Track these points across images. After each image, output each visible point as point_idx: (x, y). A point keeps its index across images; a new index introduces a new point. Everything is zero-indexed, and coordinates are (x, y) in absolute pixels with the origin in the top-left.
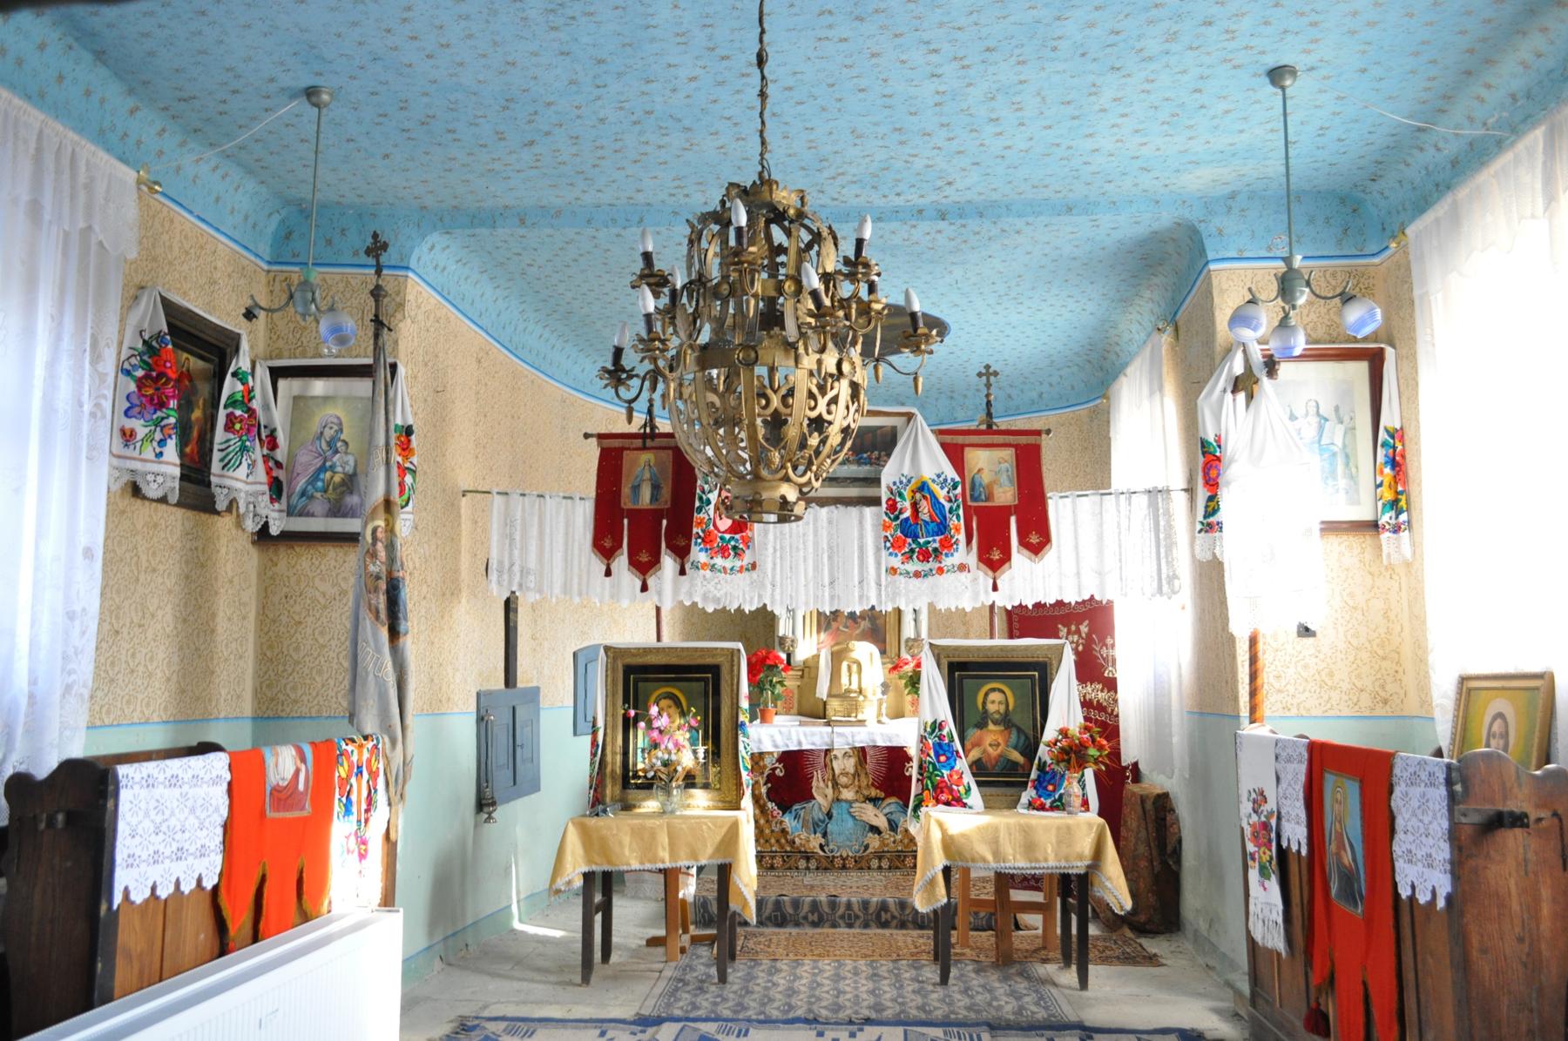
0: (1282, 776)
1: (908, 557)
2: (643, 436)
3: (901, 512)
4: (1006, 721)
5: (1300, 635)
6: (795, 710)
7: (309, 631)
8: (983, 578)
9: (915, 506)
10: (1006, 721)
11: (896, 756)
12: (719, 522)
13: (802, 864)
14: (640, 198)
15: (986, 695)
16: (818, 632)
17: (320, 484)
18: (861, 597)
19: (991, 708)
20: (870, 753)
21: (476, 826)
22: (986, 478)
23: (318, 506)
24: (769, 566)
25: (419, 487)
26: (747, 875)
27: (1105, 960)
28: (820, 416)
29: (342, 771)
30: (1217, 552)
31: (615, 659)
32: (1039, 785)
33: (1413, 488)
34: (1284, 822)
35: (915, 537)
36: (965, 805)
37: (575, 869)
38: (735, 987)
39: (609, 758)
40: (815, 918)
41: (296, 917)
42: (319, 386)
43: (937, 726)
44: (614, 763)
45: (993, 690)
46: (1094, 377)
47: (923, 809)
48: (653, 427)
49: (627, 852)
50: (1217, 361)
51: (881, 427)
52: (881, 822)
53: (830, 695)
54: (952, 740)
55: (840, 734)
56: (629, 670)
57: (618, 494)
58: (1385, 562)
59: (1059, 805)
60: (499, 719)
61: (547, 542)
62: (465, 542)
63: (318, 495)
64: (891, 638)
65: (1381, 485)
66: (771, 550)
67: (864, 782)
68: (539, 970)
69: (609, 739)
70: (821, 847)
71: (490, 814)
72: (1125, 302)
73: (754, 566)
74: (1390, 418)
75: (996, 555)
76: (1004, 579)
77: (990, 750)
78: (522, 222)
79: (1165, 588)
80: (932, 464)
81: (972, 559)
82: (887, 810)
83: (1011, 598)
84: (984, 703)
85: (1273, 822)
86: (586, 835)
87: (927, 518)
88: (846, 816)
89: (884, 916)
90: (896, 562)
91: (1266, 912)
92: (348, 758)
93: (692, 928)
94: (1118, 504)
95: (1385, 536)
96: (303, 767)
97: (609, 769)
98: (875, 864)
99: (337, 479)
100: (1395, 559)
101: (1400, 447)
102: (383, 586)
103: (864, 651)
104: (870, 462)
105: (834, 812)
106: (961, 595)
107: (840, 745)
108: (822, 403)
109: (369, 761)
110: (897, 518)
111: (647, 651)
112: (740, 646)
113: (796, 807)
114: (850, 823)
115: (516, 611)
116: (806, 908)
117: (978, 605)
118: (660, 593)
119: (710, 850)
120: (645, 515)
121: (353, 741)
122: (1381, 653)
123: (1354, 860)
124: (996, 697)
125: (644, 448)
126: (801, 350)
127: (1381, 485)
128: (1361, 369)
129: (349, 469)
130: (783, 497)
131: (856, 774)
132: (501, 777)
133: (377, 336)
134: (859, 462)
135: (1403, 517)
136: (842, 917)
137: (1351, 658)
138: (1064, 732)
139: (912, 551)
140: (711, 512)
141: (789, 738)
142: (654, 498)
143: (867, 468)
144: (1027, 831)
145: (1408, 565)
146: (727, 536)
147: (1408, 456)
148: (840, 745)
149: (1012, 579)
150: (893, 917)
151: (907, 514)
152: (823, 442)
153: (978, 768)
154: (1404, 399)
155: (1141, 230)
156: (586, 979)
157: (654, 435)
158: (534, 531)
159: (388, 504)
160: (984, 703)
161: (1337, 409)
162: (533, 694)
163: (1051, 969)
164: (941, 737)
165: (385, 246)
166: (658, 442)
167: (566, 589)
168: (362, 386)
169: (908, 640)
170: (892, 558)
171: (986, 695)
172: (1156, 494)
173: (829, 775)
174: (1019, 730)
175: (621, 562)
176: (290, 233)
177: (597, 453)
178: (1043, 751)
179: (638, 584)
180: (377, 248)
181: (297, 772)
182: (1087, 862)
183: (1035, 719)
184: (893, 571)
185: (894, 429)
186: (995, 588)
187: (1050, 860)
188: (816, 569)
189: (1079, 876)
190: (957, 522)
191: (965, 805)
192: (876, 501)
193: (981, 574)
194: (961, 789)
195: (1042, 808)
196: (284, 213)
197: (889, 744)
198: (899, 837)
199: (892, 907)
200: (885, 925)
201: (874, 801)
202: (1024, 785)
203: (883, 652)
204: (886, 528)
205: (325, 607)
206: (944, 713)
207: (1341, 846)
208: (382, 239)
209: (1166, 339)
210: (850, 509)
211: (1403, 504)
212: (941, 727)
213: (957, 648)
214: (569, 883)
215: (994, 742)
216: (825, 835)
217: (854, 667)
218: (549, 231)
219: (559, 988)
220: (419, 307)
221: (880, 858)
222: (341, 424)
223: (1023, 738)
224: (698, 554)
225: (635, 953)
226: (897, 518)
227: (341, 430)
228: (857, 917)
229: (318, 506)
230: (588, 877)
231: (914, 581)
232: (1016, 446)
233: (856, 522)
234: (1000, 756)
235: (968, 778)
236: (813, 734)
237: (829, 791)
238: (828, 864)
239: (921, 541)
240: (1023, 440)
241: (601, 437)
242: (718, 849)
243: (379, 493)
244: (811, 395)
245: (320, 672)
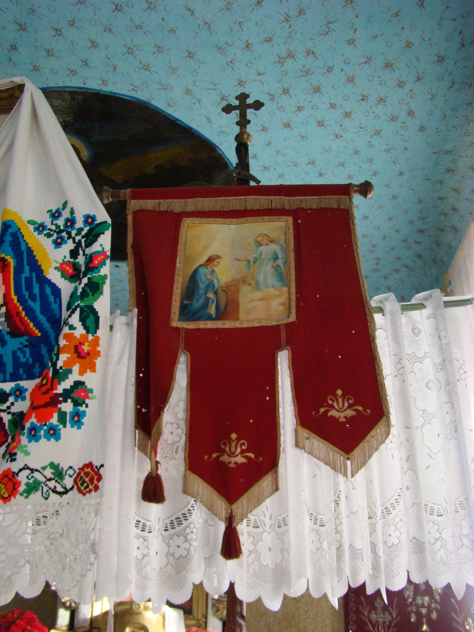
83: (281, 575)
186: (231, 548)
232: (295, 213)
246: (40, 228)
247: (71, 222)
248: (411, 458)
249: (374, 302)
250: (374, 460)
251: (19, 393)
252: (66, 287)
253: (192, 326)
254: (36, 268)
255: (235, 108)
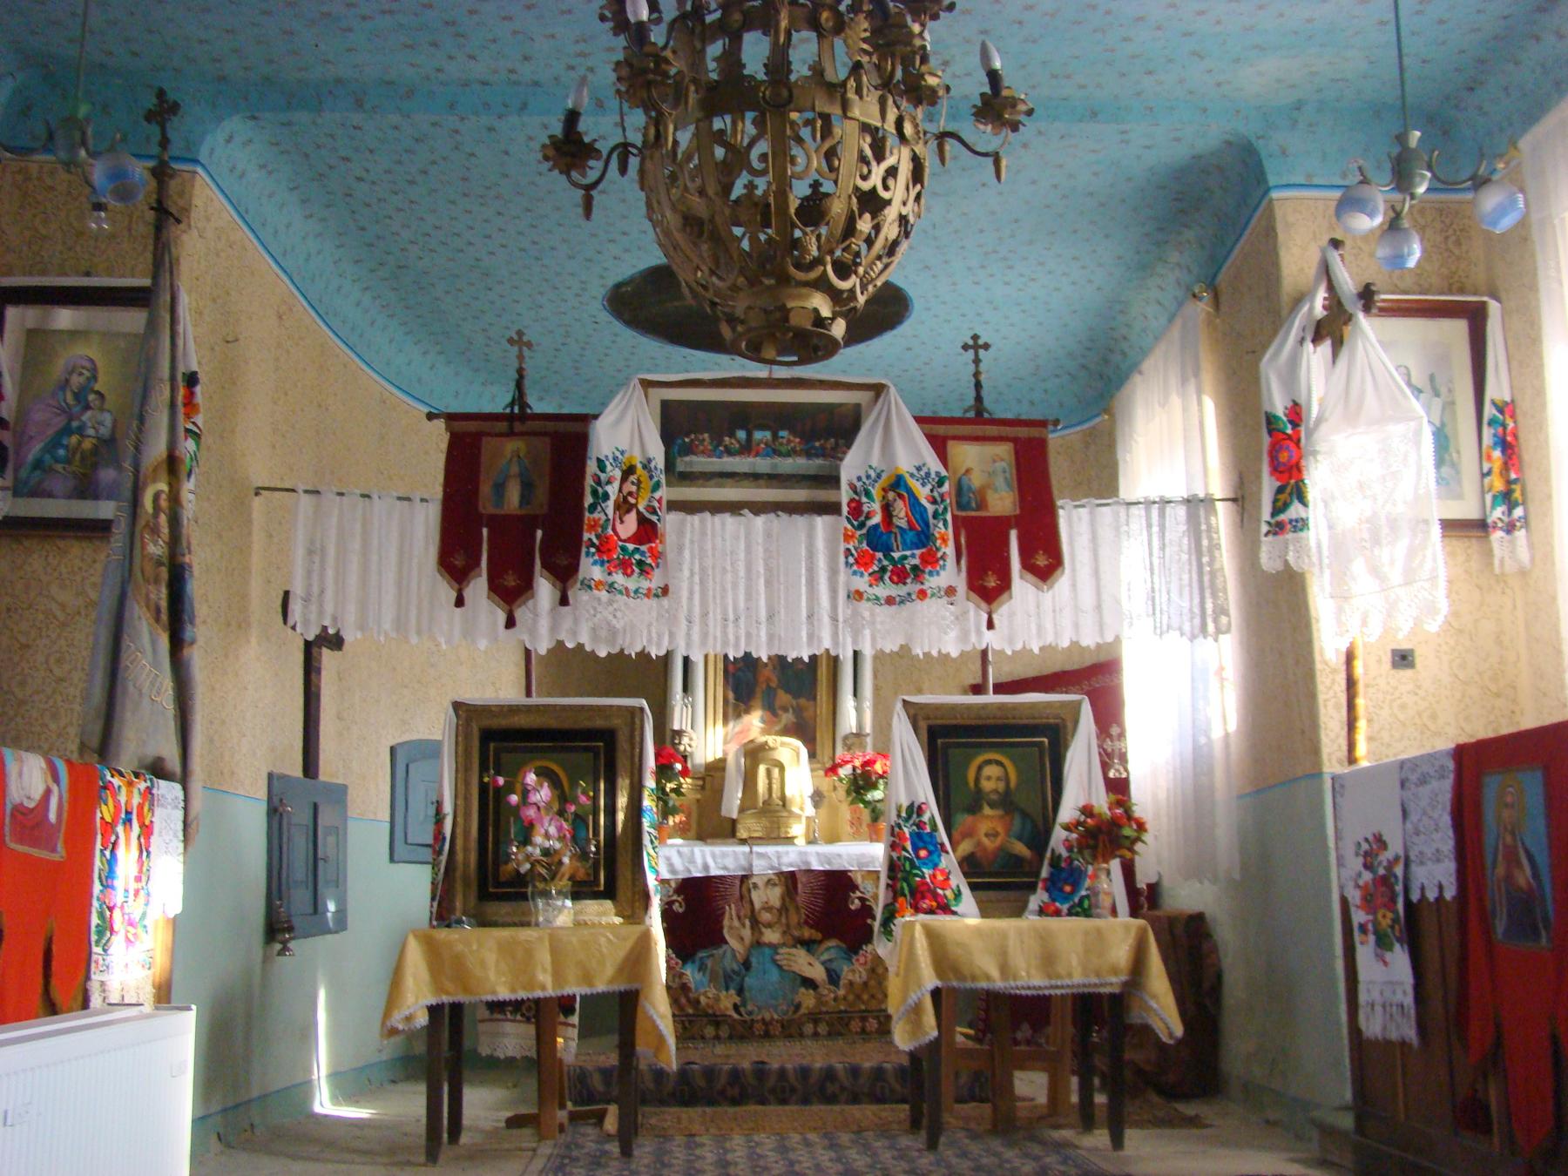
0: (1411, 807)
1: (878, 577)
2: (509, 418)
3: (868, 517)
4: (1006, 802)
5: (1395, 665)
6: (693, 832)
7: (40, 658)
8: (975, 613)
9: (887, 509)
10: (1006, 802)
11: (837, 883)
12: (619, 527)
13: (710, 1031)
14: (526, 72)
15: (980, 768)
16: (726, 720)
17: (62, 452)
18: (811, 636)
19: (987, 785)
20: (802, 879)
21: (266, 959)
22: (976, 480)
23: (59, 485)
24: (685, 594)
25: (203, 455)
26: (659, 1009)
27: (1139, 1125)
28: (874, 189)
29: (105, 812)
30: (1291, 558)
31: (468, 721)
32: (1053, 886)
33: (1531, 476)
34: (1414, 868)
35: (887, 551)
36: (954, 913)
37: (417, 999)
38: (646, 1161)
39: (460, 857)
40: (736, 1091)
41: (39, 1002)
42: (64, 318)
43: (915, 810)
44: (466, 864)
45: (989, 762)
46: (1100, 380)
47: (899, 921)
48: (524, 406)
49: (492, 976)
50: (1284, 312)
51: (841, 405)
52: (817, 972)
53: (742, 810)
54: (934, 828)
55: (761, 855)
56: (487, 736)
57: (475, 492)
58: (1497, 570)
59: (1083, 909)
60: (298, 815)
61: (375, 558)
62: (256, 561)
63: (59, 467)
64: (822, 736)
65: (1489, 473)
66: (686, 573)
67: (794, 919)
68: (355, 1151)
69: (459, 831)
70: (736, 1007)
71: (284, 943)
72: (1143, 268)
73: (665, 591)
74: (1497, 389)
75: (992, 582)
76: (1001, 614)
77: (986, 841)
78: (359, 104)
79: (1211, 627)
80: (911, 453)
81: (961, 583)
82: (825, 957)
83: (1011, 641)
84: (977, 780)
85: (1399, 870)
86: (433, 952)
87: (903, 524)
88: (769, 965)
89: (831, 1088)
90: (862, 583)
91: (1387, 994)
92: (114, 796)
93: (569, 1105)
94: (1148, 518)
95: (1497, 536)
96: (55, 789)
97: (459, 874)
98: (809, 1028)
99: (87, 444)
100: (1510, 567)
101: (1511, 425)
102: (164, 573)
103: (790, 752)
104: (823, 453)
105: (754, 960)
106: (942, 626)
107: (760, 868)
108: (878, 172)
109: (140, 807)
110: (862, 525)
111: (513, 710)
112: (644, 703)
113: (702, 954)
114: (774, 975)
115: (319, 671)
116: (723, 1080)
117: (969, 648)
118: (533, 631)
119: (610, 970)
120: (517, 509)
121: (121, 774)
122: (1494, 688)
123: (1536, 875)
124: (992, 772)
125: (511, 434)
126: (851, 95)
127: (1489, 473)
128: (1457, 329)
129: (104, 432)
130: (816, 311)
131: (784, 909)
132: (299, 899)
133: (159, 228)
134: (809, 454)
135: (1518, 512)
136: (773, 1091)
137: (1458, 695)
138: (1087, 810)
139: (883, 569)
140: (610, 511)
141: (692, 861)
142: (525, 499)
143: (819, 461)
144: (1044, 938)
145: (1523, 573)
146: (631, 547)
147: (1521, 435)
148: (760, 868)
149: (1012, 615)
150: (843, 1088)
151: (877, 519)
152: (877, 228)
153: (970, 866)
154: (1514, 364)
155: (1180, 153)
156: (432, 1154)
157: (524, 416)
158: (356, 545)
159: (172, 463)
160: (977, 780)
161: (1432, 378)
162: (339, 794)
163: (1066, 1134)
164: (920, 825)
165: (174, 108)
166: (531, 425)
167: (400, 624)
168: (131, 320)
169: (846, 738)
170: (857, 578)
171: (980, 768)
172: (1197, 505)
173: (746, 911)
174: (1025, 815)
175: (478, 587)
176: (29, 108)
177: (446, 437)
178: (1059, 836)
179: (502, 617)
180: (164, 110)
181: (48, 792)
182: (1124, 978)
183: (1045, 799)
184: (859, 595)
185: (858, 406)
186: (990, 625)
187: (1075, 974)
188: (749, 596)
189: (1112, 996)
190: (944, 530)
191: (954, 913)
192: (832, 509)
193: (971, 606)
194: (949, 893)
195: (1057, 913)
196: (20, 77)
197: (827, 868)
198: (841, 992)
199: (842, 1074)
200: (831, 1099)
201: (808, 945)
202: (1032, 888)
203: (812, 755)
204: (847, 538)
205: (64, 625)
206: (924, 792)
207: (1512, 858)
208: (172, 96)
209: (1202, 308)
210: (796, 517)
211: (1517, 495)
212: (920, 811)
213: (938, 707)
214: (408, 1019)
215: (990, 830)
216: (740, 992)
217: (776, 772)
218: (395, 119)
219: (395, 1170)
220: (208, 220)
221: (816, 1022)
222: (94, 370)
223: (1029, 826)
224: (591, 569)
225: (494, 1134)
226: (862, 525)
227: (95, 378)
228: (793, 1090)
229: (59, 485)
230: (433, 1010)
231: (887, 609)
232: (1015, 440)
233: (803, 538)
234: (1000, 849)
235: (958, 880)
236: (724, 855)
237: (747, 933)
238: (743, 1031)
239: (896, 555)
240: (1022, 432)
241: (451, 418)
242: (620, 970)
243: (157, 449)
244: (863, 159)
245: (55, 716)
246: (912, 475)
247: (928, 474)
248: (1074, 586)
249: (1059, 503)
250: (1056, 586)
251: (913, 556)
252: (930, 508)
253: (964, 514)
254: (916, 499)
255: (976, 354)
